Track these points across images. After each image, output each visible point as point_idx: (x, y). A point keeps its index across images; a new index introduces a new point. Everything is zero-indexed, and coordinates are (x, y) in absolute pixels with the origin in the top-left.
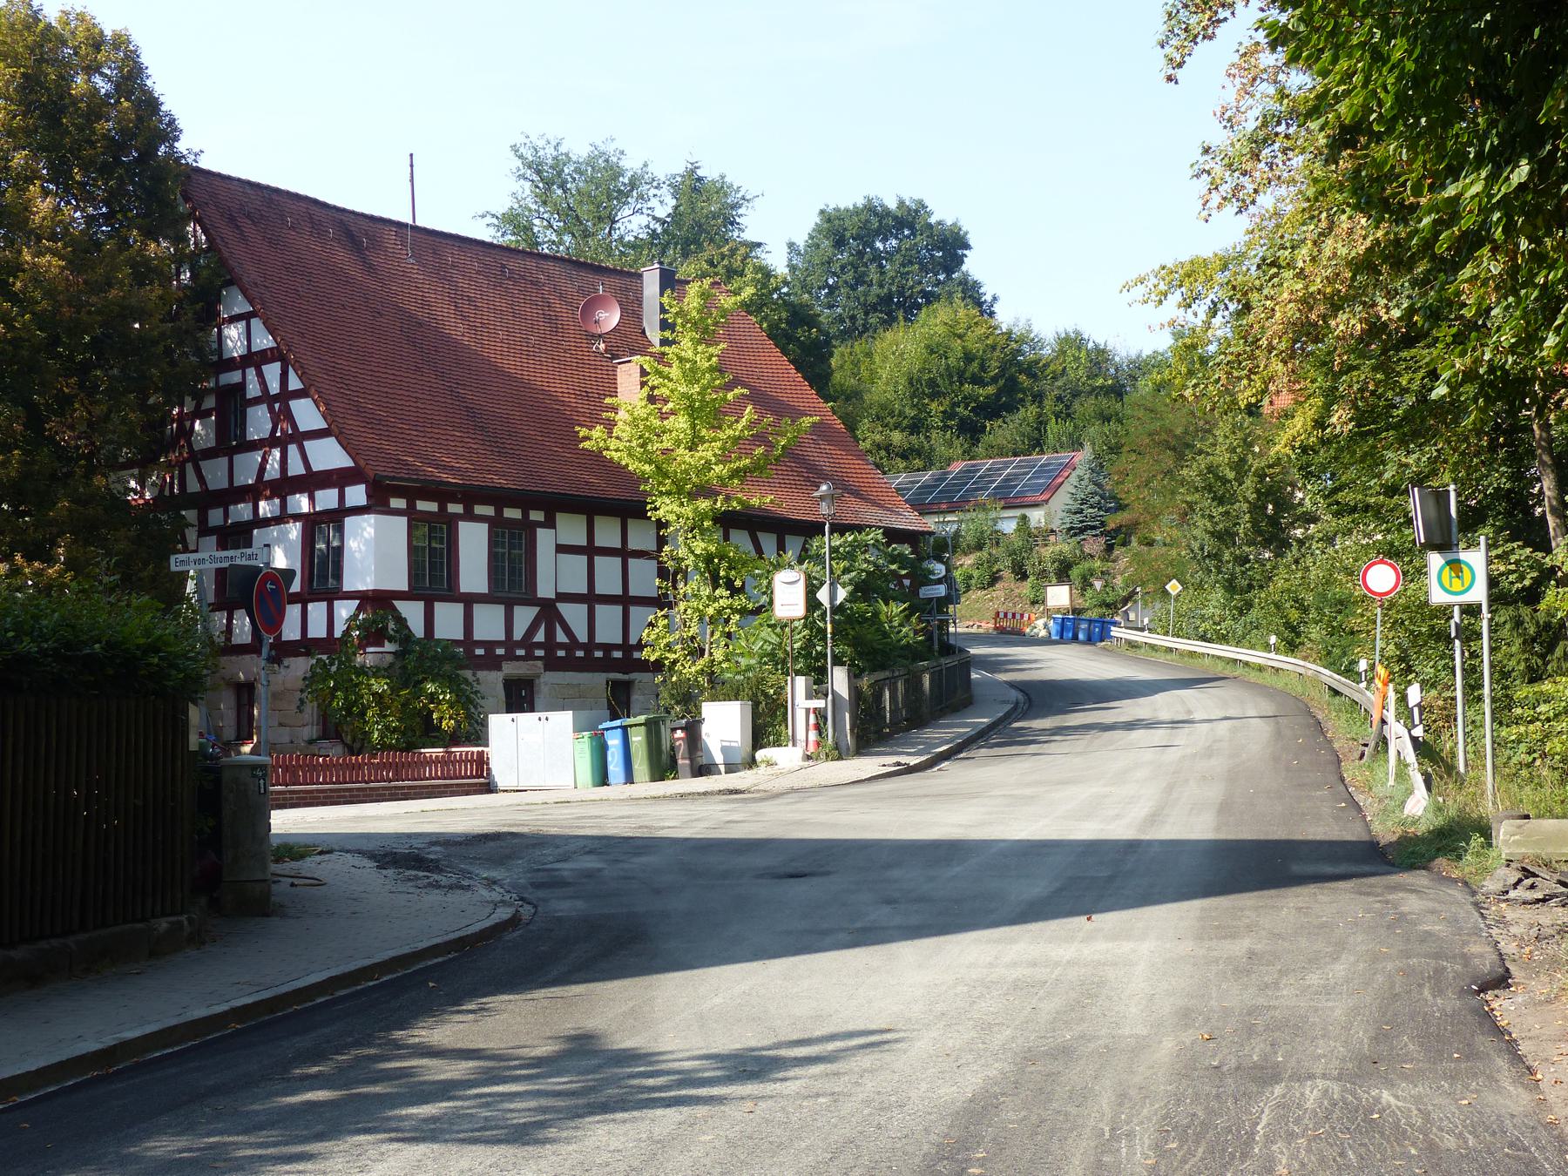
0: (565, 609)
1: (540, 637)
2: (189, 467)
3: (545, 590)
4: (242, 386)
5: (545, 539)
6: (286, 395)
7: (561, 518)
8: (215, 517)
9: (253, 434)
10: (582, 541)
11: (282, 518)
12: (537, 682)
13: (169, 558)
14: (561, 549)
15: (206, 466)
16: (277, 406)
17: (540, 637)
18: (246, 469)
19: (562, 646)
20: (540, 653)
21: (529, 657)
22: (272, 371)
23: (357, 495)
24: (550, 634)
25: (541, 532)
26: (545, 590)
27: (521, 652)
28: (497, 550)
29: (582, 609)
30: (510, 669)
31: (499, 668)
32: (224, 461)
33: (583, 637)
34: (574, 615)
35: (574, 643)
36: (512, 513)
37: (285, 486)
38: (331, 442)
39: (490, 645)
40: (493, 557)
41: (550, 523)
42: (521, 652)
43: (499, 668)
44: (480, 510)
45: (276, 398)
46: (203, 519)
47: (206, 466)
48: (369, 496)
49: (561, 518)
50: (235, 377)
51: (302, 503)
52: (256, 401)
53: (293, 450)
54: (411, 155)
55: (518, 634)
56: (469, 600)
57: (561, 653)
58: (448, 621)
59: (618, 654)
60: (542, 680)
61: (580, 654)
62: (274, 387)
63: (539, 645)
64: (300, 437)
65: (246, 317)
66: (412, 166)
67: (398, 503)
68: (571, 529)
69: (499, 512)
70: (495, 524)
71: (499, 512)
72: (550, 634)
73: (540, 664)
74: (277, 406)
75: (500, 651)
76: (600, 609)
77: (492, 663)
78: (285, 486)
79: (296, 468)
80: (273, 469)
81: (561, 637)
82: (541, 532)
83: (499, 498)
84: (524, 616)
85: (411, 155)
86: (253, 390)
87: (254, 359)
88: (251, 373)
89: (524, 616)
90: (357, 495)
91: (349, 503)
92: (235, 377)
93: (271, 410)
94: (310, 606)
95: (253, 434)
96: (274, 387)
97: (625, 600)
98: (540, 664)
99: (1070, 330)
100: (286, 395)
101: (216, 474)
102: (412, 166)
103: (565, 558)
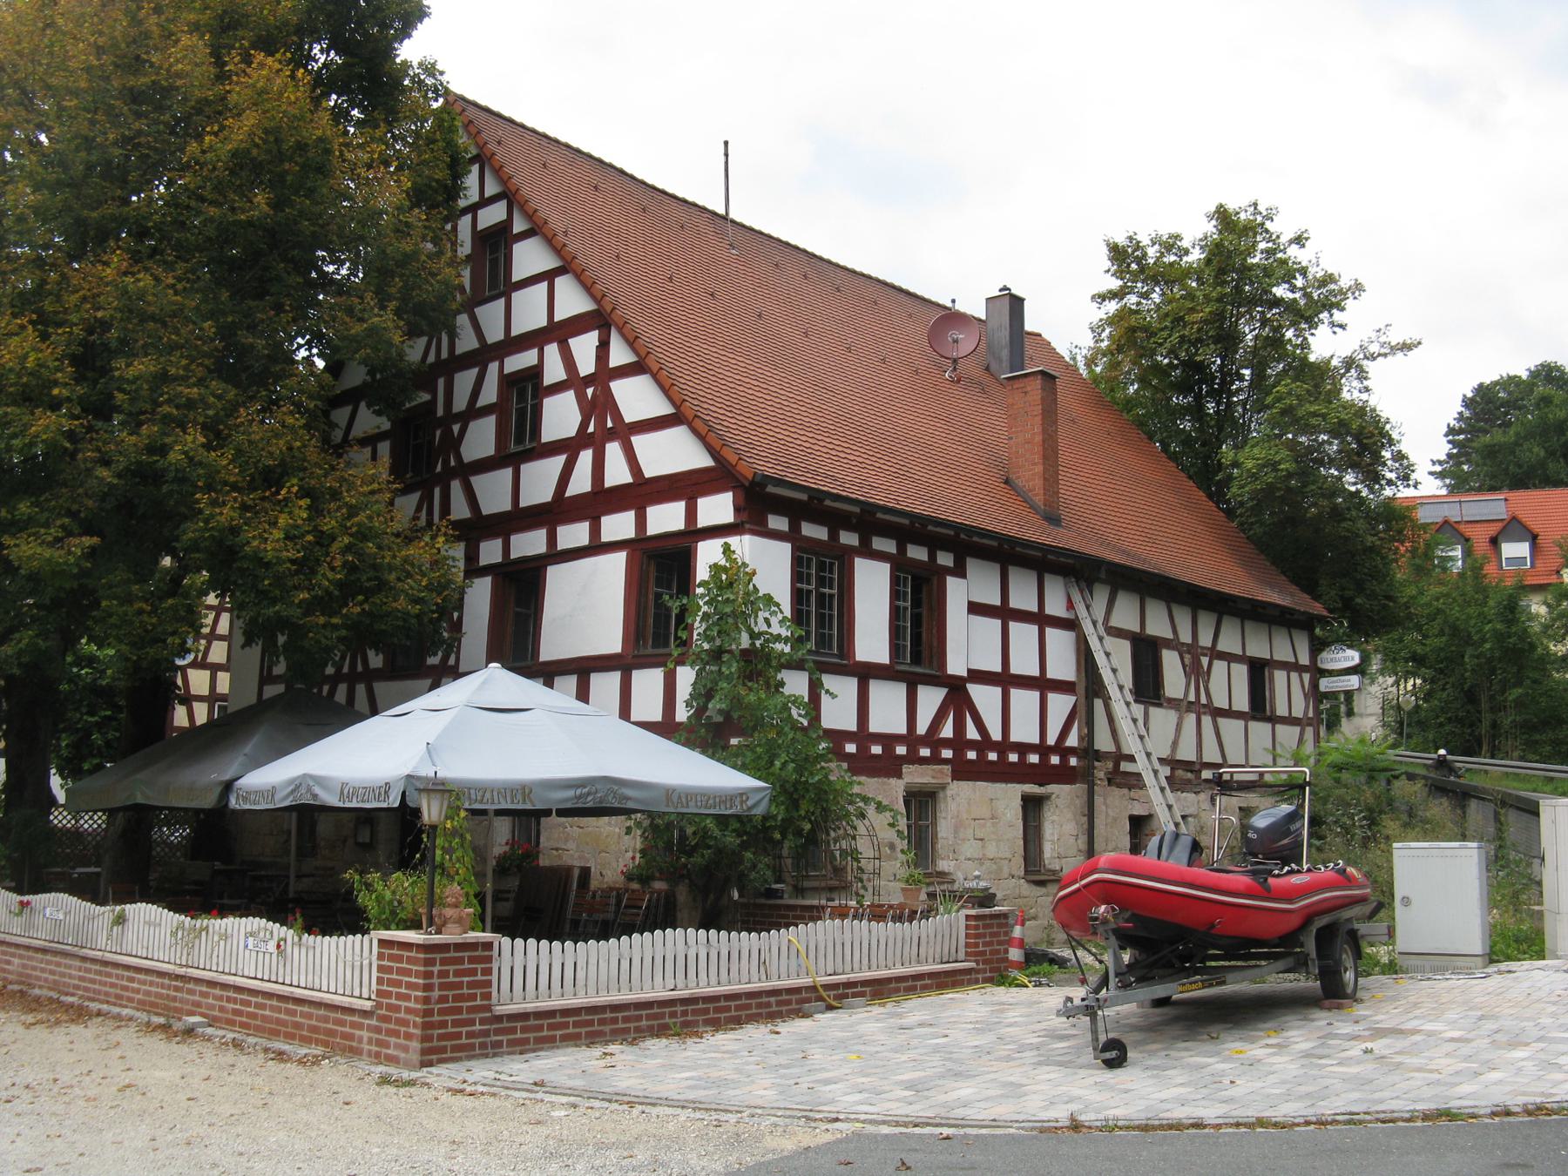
0: (977, 692)
1: (947, 731)
2: (456, 486)
3: (956, 666)
4: (536, 372)
5: (957, 594)
6: (605, 373)
7: (972, 565)
8: (490, 552)
9: (550, 433)
10: (995, 600)
11: (597, 547)
12: (941, 795)
13: (234, 811)
14: (975, 608)
15: (478, 482)
16: (590, 391)
17: (947, 731)
18: (540, 480)
19: (972, 744)
20: (947, 754)
21: (935, 759)
22: (584, 347)
23: (717, 508)
24: (959, 727)
25: (952, 583)
26: (956, 666)
27: (925, 752)
28: (898, 603)
29: (997, 692)
30: (915, 776)
31: (899, 775)
32: (507, 473)
33: (996, 735)
34: (985, 698)
35: (985, 743)
36: (918, 553)
37: (603, 500)
38: (679, 434)
39: (888, 740)
40: (895, 613)
41: (959, 571)
42: (925, 752)
43: (899, 775)
44: (879, 544)
45: (589, 380)
46: (472, 556)
47: (478, 482)
48: (737, 509)
49: (972, 565)
50: (528, 358)
51: (619, 525)
52: (558, 388)
53: (613, 450)
54: (726, 143)
55: (922, 728)
56: (866, 674)
57: (972, 755)
58: (838, 710)
59: (1034, 758)
60: (949, 793)
61: (993, 756)
62: (586, 366)
63: (946, 743)
64: (625, 432)
65: (549, 276)
66: (726, 155)
67: (778, 523)
68: (979, 584)
69: (902, 549)
70: (900, 566)
71: (902, 549)
72: (959, 727)
73: (947, 768)
74: (590, 391)
75: (901, 750)
76: (1016, 694)
77: (889, 766)
78: (603, 500)
79: (617, 473)
80: (581, 483)
81: (972, 733)
82: (952, 583)
83: (912, 528)
84: (930, 699)
85: (726, 143)
86: (554, 371)
87: (559, 332)
88: (552, 351)
89: (930, 699)
90: (717, 508)
91: (703, 521)
92: (528, 358)
93: (581, 397)
94: (637, 675)
95: (550, 433)
96: (586, 366)
97: (1005, 680)
98: (947, 768)
99: (1505, 375)
100: (605, 373)
101: (494, 493)
102: (726, 155)
103: (980, 621)
